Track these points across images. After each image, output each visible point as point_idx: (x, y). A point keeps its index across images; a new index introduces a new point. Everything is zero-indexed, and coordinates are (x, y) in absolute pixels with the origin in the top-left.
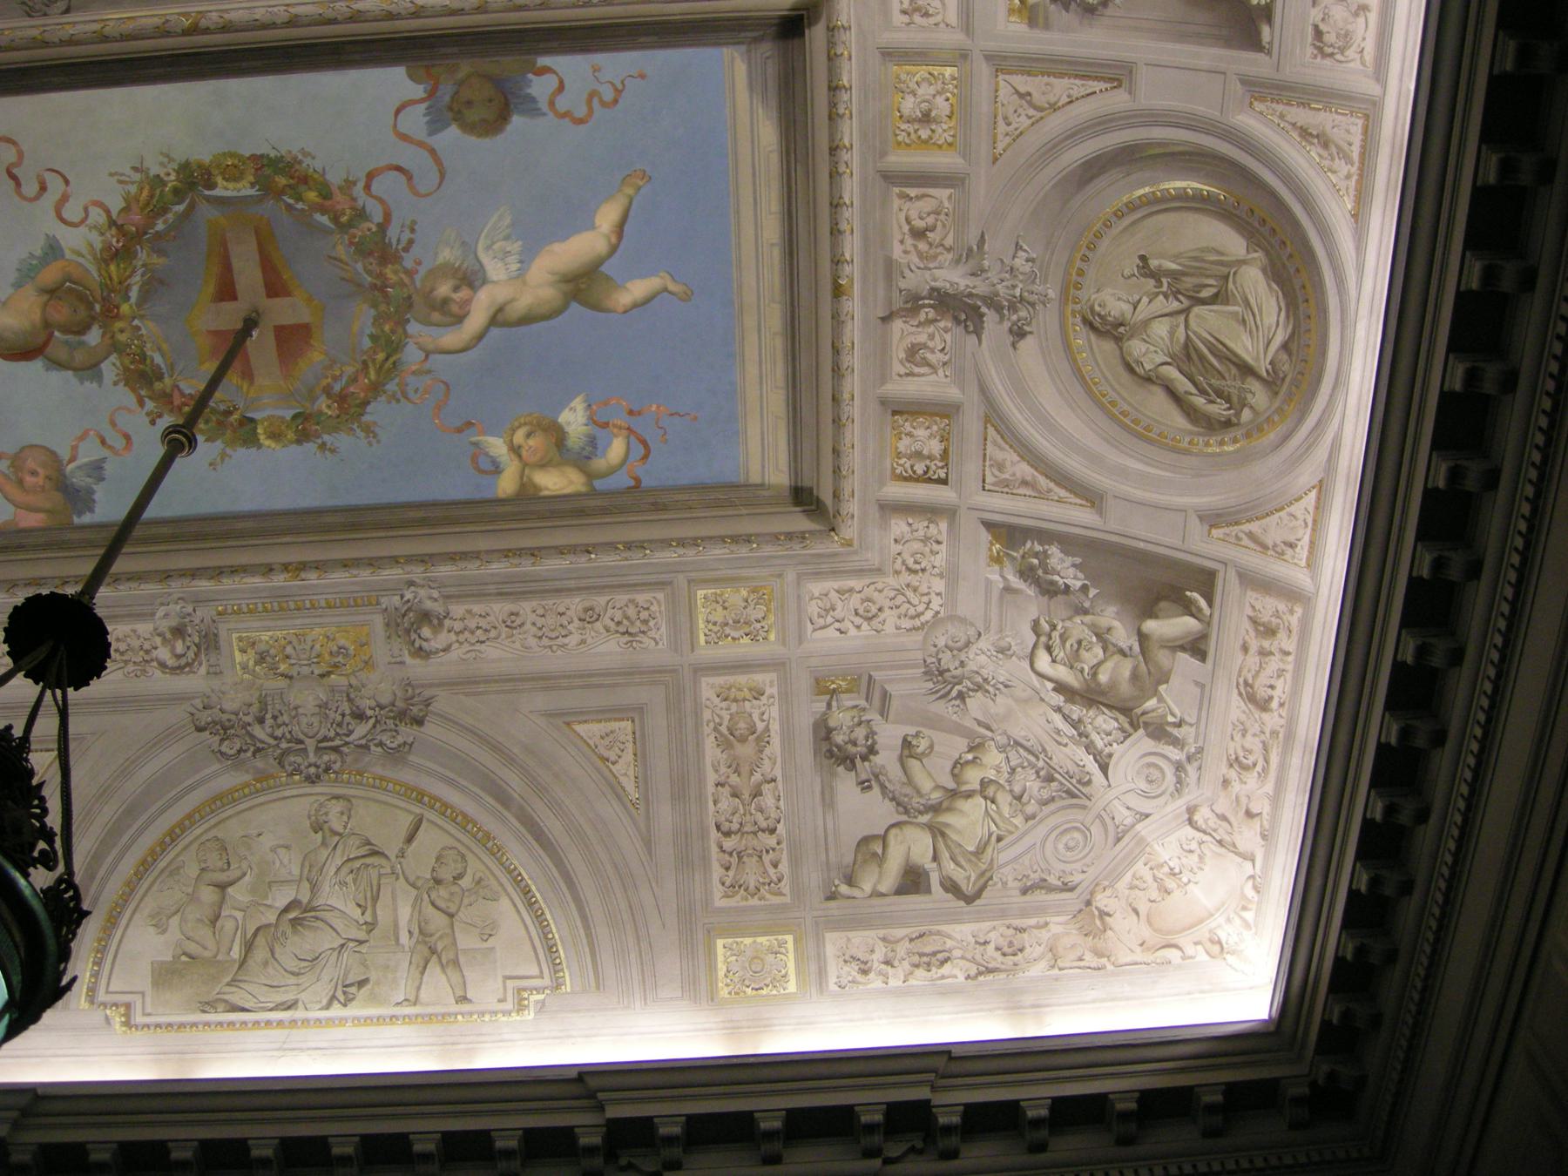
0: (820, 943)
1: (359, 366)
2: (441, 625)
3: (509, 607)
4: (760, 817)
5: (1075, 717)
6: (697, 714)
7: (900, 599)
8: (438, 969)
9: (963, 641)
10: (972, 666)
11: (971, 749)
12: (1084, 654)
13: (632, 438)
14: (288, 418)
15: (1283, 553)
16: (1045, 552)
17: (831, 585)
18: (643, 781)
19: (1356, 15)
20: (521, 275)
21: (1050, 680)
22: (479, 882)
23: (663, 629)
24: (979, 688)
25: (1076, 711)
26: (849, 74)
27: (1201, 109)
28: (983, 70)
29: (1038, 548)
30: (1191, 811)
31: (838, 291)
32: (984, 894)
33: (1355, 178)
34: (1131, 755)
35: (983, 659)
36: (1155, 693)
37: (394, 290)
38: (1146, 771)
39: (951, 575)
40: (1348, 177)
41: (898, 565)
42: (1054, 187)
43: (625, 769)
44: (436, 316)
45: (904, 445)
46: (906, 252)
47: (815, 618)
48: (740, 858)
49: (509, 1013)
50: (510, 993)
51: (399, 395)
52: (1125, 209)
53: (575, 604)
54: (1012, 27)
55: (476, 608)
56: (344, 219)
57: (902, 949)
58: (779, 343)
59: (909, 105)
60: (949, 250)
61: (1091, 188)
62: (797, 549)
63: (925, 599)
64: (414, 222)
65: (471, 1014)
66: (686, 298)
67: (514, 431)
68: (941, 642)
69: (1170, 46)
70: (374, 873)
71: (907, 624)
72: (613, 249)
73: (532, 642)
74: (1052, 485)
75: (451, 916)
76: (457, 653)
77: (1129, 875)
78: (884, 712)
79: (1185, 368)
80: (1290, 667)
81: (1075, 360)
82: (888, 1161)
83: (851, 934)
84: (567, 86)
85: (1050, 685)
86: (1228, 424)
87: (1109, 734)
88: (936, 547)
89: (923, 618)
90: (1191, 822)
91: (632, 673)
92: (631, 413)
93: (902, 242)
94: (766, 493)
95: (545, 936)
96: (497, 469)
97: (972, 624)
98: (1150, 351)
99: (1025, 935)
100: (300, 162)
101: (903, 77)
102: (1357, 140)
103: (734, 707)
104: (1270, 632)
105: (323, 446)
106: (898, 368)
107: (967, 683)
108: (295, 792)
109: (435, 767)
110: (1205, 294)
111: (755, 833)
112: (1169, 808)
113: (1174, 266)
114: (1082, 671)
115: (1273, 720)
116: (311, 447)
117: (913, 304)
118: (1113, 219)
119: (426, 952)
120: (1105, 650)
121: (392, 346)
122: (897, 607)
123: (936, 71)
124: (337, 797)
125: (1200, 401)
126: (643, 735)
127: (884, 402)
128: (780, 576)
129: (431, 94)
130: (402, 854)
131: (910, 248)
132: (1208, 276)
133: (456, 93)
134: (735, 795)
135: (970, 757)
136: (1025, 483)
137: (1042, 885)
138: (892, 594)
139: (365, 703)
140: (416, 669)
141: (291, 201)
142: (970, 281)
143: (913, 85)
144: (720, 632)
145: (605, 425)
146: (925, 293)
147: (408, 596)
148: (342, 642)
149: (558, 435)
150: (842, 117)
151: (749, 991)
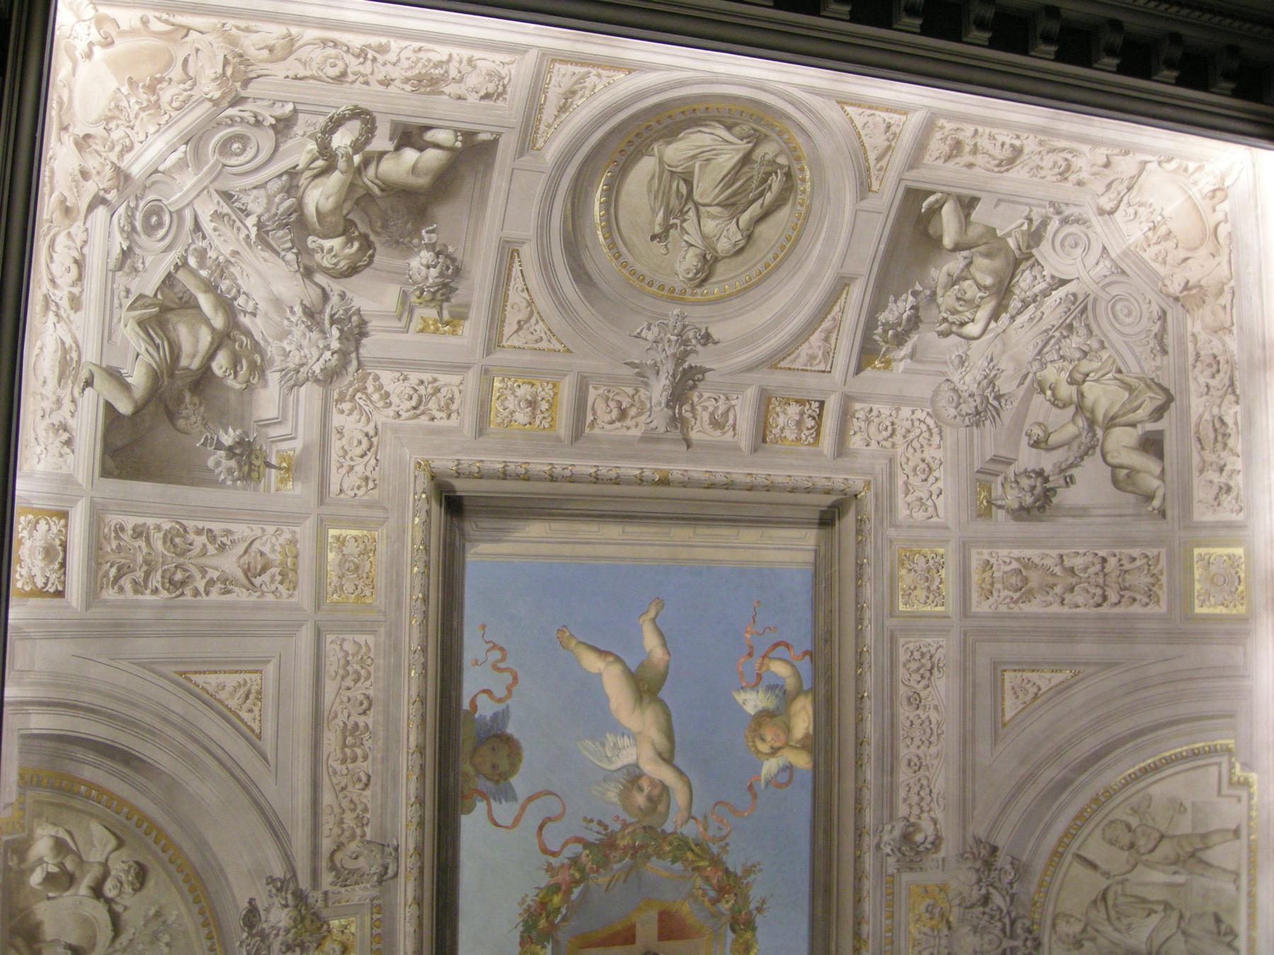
0: (1202, 526)
1: (696, 874)
2: (913, 825)
4: (1092, 570)
5: (1020, 305)
6: (1001, 617)
7: (915, 444)
9: (951, 394)
10: (974, 388)
11: (1043, 391)
12: (968, 296)
13: (771, 655)
14: (734, 936)
15: (894, 134)
16: (883, 324)
17: (900, 500)
19: (475, 67)
20: (634, 736)
21: (988, 324)
23: (929, 640)
25: (1015, 304)
26: (494, 462)
28: (498, 357)
29: (880, 330)
30: (1102, 212)
32: (1165, 385)
33: (600, 71)
35: (968, 378)
36: (1003, 239)
37: (641, 837)
38: (1067, 248)
39: (898, 401)
40: (599, 76)
43: (1045, 680)
44: (661, 808)
45: (790, 435)
46: (637, 426)
47: (929, 514)
48: (1126, 589)
51: (722, 843)
53: (904, 712)
54: (466, 333)
55: (902, 793)
56: (577, 875)
57: (1209, 457)
58: (703, 531)
59: (521, 417)
60: (637, 391)
61: (596, 277)
62: (870, 526)
63: (916, 423)
64: (585, 819)
65: (1249, 827)
66: (661, 603)
67: (758, 752)
68: (952, 412)
70: (1121, 899)
71: (936, 439)
72: (618, 659)
73: (933, 750)
74: (829, 317)
75: (1162, 837)
76: (939, 814)
77: (1154, 265)
78: (1008, 462)
79: (741, 208)
80: (988, 130)
81: (731, 295)
83: (1196, 499)
85: (993, 324)
86: (788, 175)
87: (1035, 278)
88: (874, 413)
89: (932, 425)
90: (1111, 213)
91: (965, 669)
92: (750, 655)
93: (628, 428)
95: (1183, 758)
96: (789, 768)
97: (940, 385)
98: (727, 235)
99: (1202, 353)
100: (529, 907)
101: (499, 420)
102: (571, 68)
104: (958, 145)
105: (759, 910)
107: (987, 392)
110: (684, 190)
112: (1099, 230)
113: (661, 214)
114: (982, 298)
115: (1030, 144)
116: (759, 920)
117: (678, 422)
119: (1192, 861)
121: (683, 845)
123: (496, 394)
124: (1054, 926)
125: (769, 197)
126: (1018, 663)
127: (755, 450)
128: (891, 541)
129: (484, 796)
130: (1106, 874)
131: (634, 422)
132: (671, 187)
134: (1072, 590)
135: (1049, 393)
136: (827, 339)
137: (1160, 337)
138: (911, 450)
139: (976, 894)
140: (949, 848)
141: (559, 917)
142: (663, 375)
143: (506, 413)
144: (935, 594)
145: (759, 676)
147: (888, 850)
148: (923, 908)
149: (764, 716)
150: (527, 471)
151: (1241, 588)
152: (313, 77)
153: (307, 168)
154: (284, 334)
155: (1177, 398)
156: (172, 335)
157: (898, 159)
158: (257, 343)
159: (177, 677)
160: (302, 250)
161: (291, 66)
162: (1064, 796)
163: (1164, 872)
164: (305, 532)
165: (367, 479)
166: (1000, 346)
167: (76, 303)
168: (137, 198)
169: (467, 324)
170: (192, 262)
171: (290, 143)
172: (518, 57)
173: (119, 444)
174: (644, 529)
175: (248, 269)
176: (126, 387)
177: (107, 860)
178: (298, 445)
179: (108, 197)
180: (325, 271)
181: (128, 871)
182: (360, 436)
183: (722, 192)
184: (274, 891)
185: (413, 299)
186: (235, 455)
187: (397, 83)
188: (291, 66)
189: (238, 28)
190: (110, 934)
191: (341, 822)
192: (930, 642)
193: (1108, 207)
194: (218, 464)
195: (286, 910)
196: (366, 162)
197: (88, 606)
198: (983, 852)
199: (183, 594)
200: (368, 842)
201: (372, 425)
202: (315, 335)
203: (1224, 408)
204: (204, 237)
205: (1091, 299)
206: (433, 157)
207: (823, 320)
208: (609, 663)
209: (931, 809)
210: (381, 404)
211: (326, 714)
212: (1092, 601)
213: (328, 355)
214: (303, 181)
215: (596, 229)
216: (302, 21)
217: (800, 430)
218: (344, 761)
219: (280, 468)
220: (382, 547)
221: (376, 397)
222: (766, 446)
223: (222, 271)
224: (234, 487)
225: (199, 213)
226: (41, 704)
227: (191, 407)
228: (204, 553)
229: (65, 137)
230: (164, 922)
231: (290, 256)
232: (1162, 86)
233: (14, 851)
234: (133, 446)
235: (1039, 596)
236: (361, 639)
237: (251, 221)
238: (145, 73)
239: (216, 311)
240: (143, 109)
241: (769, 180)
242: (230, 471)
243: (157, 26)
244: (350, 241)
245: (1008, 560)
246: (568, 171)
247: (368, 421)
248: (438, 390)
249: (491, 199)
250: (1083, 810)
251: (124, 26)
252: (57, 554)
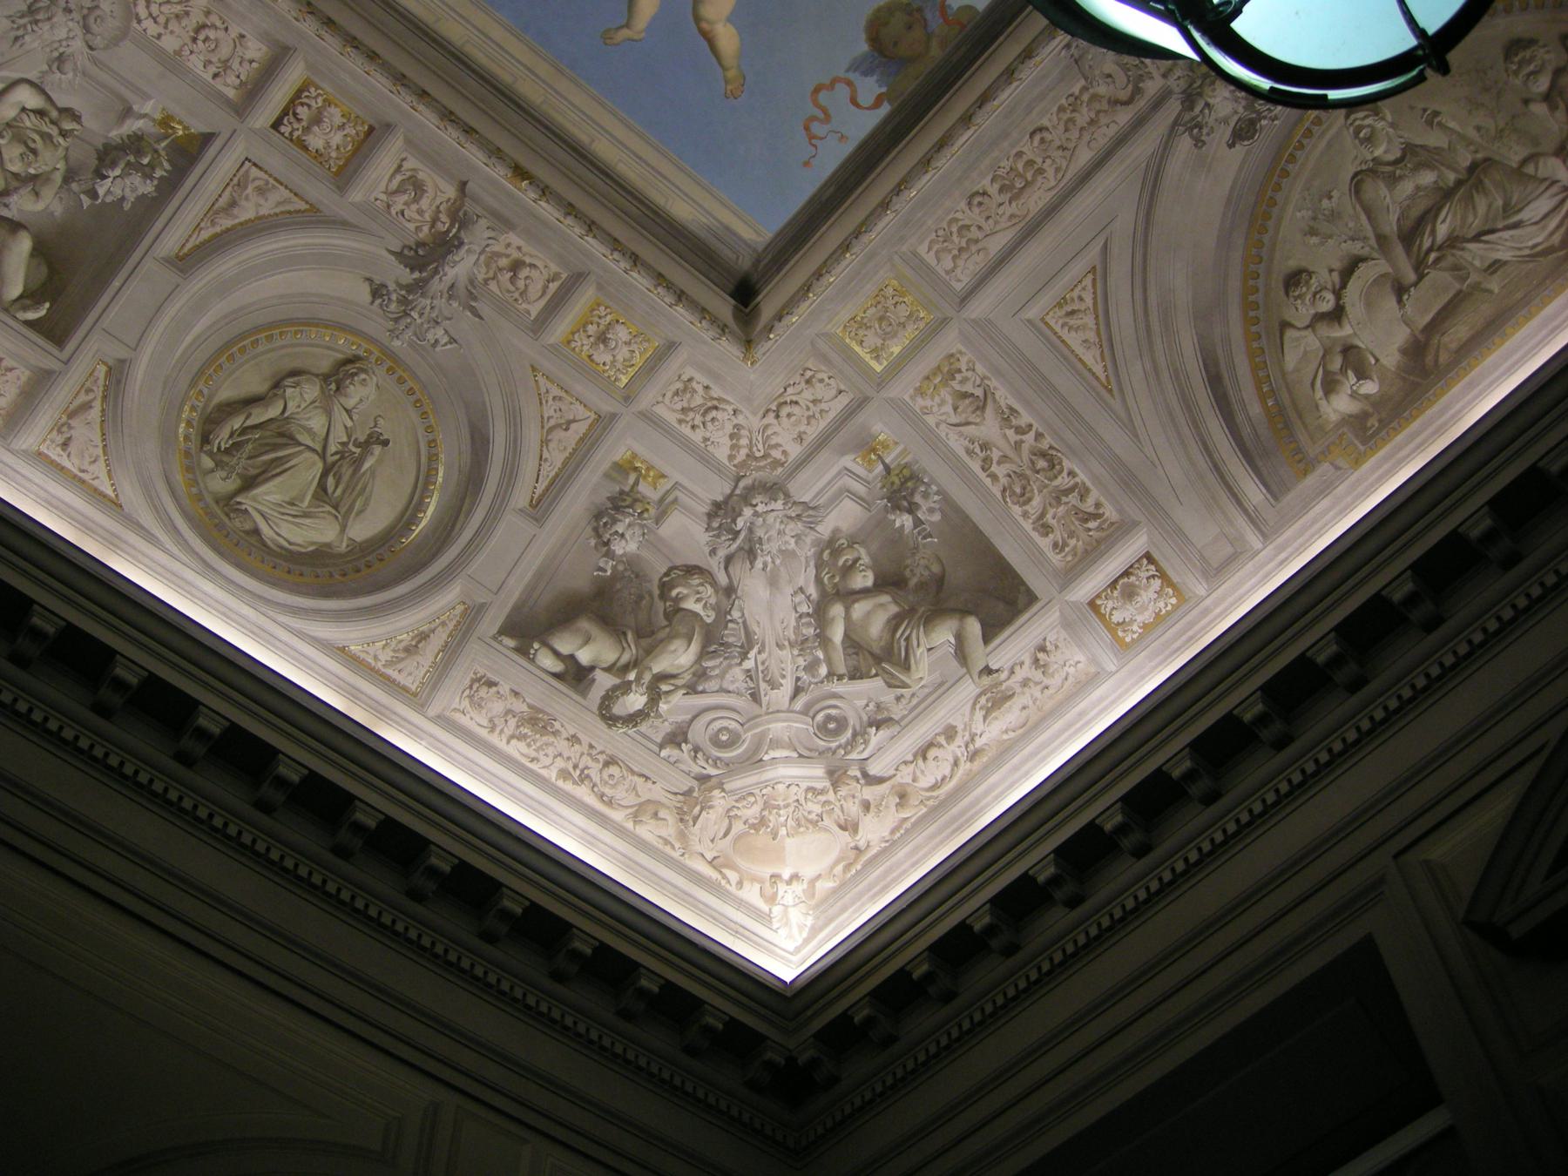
10: (60, 18)
12: (18, 150)
15: (60, 432)
16: (152, 178)
19: (491, 720)
27: (481, 558)
28: (607, 407)
29: (159, 173)
35: (62, 33)
40: (376, 658)
41: (214, 19)
42: (484, 404)
46: (508, 245)
52: (433, 451)
54: (623, 449)
58: (506, 78)
59: (622, 333)
60: (486, 281)
61: (465, 432)
63: (162, 20)
66: (606, 36)
69: (538, 562)
72: (697, 19)
74: (218, 229)
79: (273, 426)
81: (327, 327)
84: (853, 108)
86: (205, 439)
88: (212, 70)
93: (519, 248)
97: (106, 48)
98: (301, 398)
101: (646, 345)
110: (331, 481)
113: (366, 465)
117: (461, 219)
118: (431, 437)
120: (16, 176)
123: (632, 371)
125: (237, 423)
127: (388, 127)
132: (344, 492)
133: (925, 27)
142: (448, 280)
143: (634, 347)
152: (633, 772)
153: (677, 688)
154: (787, 554)
156: (886, 636)
157: (62, 394)
158: (817, 567)
159: (1115, 392)
160: (723, 614)
161: (648, 791)
164: (901, 389)
165: (808, 382)
167: (950, 733)
168: (834, 753)
169: (617, 458)
170: (823, 670)
171: (680, 718)
172: (447, 714)
173: (1001, 607)
174: (568, 126)
175: (779, 628)
176: (959, 637)
177: (1307, 327)
178: (847, 461)
179: (858, 774)
180: (714, 584)
181: (1299, 297)
182: (784, 420)
184: (1205, 131)
185: (652, 511)
186: (910, 503)
187: (565, 735)
188: (648, 791)
189: (673, 847)
190: (1362, 266)
191: (1092, 122)
194: (931, 511)
195: (1211, 101)
196: (626, 668)
197: (1135, 524)
199: (1051, 447)
200: (1086, 79)
201: (765, 421)
202: (760, 533)
204: (798, 679)
206: (565, 644)
207: (228, 230)
208: (708, 22)
210: (744, 432)
211: (1018, 228)
213: (760, 508)
214: (687, 677)
216: (619, 831)
217: (320, 111)
218: (1041, 171)
219: (880, 457)
220: (844, 315)
221: (744, 442)
222: (372, 122)
223: (803, 642)
224: (933, 481)
225: (787, 699)
226: (1239, 503)
227: (918, 571)
228: (1004, 459)
229: (862, 844)
230: (1314, 219)
231: (736, 614)
233: (1365, 429)
234: (997, 597)
236: (930, 259)
237: (749, 664)
238: (762, 838)
239: (833, 619)
240: (778, 808)
242: (926, 495)
243: (733, 876)
244: (678, 599)
247: (766, 427)
248: (683, 410)
249: (530, 574)
251: (757, 886)
252: (1123, 585)
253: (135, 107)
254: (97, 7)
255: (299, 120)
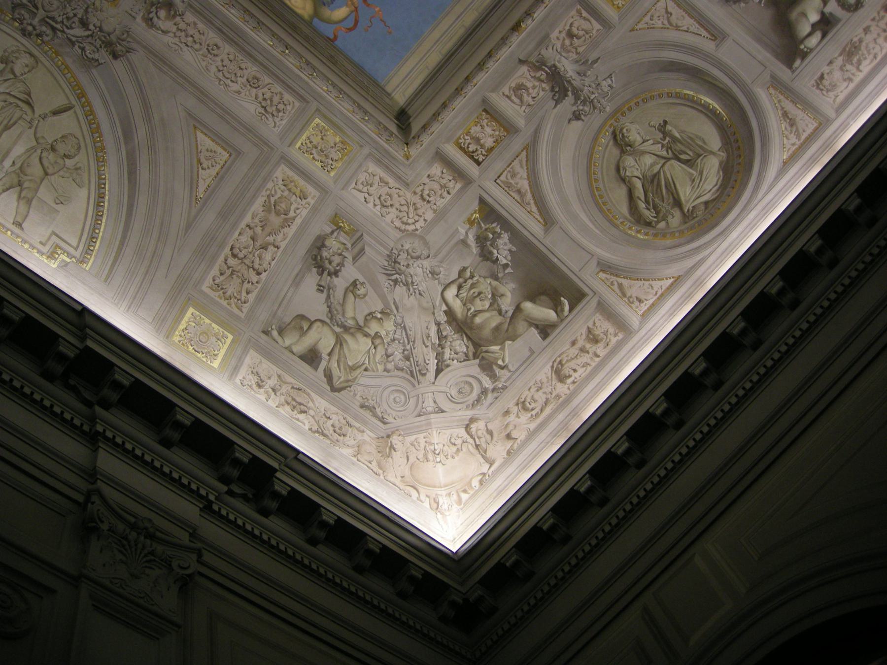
0: (245, 352)
2: (174, 17)
3: (218, 40)
4: (257, 261)
5: (444, 334)
6: (265, 181)
7: (405, 208)
8: (15, 196)
9: (418, 254)
10: (411, 270)
11: (382, 312)
12: (478, 301)
13: (353, 15)
15: (632, 303)
16: (500, 234)
17: (380, 172)
18: (211, 191)
19: (845, 80)
21: (447, 304)
22: (76, 169)
23: (284, 122)
24: (406, 284)
25: (448, 330)
29: (498, 230)
30: (472, 420)
31: (516, 27)
32: (342, 392)
33: (796, 147)
34: (462, 371)
35: (420, 270)
36: (502, 343)
38: (462, 385)
39: (440, 215)
40: (793, 144)
41: (418, 190)
42: (649, 62)
43: (206, 177)
45: (475, 130)
46: (558, 38)
47: (359, 183)
48: (232, 274)
49: (42, 254)
50: (50, 243)
53: (252, 69)
55: (201, 26)
57: (285, 388)
58: (462, 31)
60: (577, 53)
61: (665, 75)
63: (417, 218)
65: (18, 236)
70: (18, 114)
71: (398, 223)
73: (213, 69)
74: (532, 202)
75: (46, 174)
76: (168, 39)
77: (414, 437)
78: (355, 259)
79: (647, 185)
80: (594, 364)
82: (230, 493)
83: (264, 360)
85: (444, 308)
86: (649, 224)
87: (456, 353)
88: (445, 194)
89: (407, 227)
90: (467, 427)
93: (560, 32)
94: (387, 100)
95: (94, 229)
97: (429, 249)
98: (633, 167)
99: (350, 429)
102: (809, 131)
103: (286, 193)
104: (595, 340)
106: (506, 90)
107: (403, 277)
108: (8, 31)
109: (103, 86)
110: (683, 157)
111: (249, 267)
112: (460, 413)
113: (677, 135)
114: (469, 310)
115: (562, 389)
118: (665, 95)
119: (16, 181)
120: (491, 305)
122: (400, 211)
125: (642, 205)
126: (230, 167)
127: (485, 101)
128: (361, 146)
130: (44, 117)
134: (253, 239)
135: (379, 316)
136: (519, 192)
137: (372, 409)
138: (404, 202)
139: (93, 20)
140: (139, 27)
142: (575, 76)
146: (549, 64)
151: (191, 348)
155: (332, 394)
162: (120, 131)
163: (19, 157)
166: (425, 305)
172: (836, 106)
183: (666, 179)
187: (863, 35)
192: (283, 122)
193: (474, 427)
198: (119, 48)
203: (311, 419)
205: (416, 383)
206: (804, 29)
209: (175, 36)
212: (238, 246)
215: (695, 92)
222: (481, 110)
232: (578, 478)
235: (262, 214)
241: (658, 213)
245: (298, 212)
246: (743, 96)
250: (101, 136)
253: (462, 238)
254: (407, 251)
255: (477, 150)
